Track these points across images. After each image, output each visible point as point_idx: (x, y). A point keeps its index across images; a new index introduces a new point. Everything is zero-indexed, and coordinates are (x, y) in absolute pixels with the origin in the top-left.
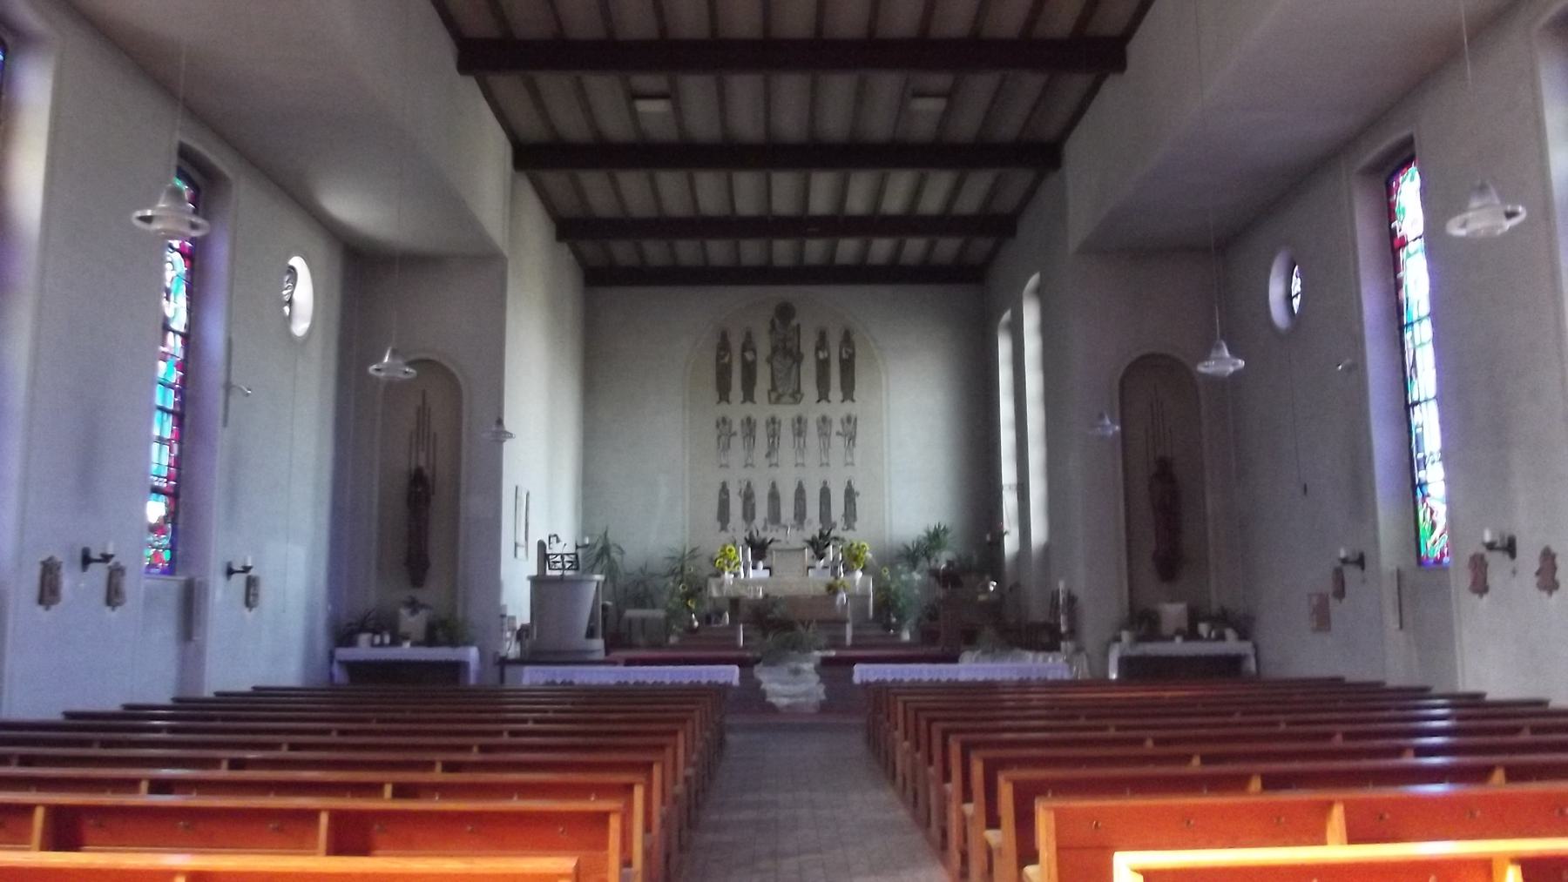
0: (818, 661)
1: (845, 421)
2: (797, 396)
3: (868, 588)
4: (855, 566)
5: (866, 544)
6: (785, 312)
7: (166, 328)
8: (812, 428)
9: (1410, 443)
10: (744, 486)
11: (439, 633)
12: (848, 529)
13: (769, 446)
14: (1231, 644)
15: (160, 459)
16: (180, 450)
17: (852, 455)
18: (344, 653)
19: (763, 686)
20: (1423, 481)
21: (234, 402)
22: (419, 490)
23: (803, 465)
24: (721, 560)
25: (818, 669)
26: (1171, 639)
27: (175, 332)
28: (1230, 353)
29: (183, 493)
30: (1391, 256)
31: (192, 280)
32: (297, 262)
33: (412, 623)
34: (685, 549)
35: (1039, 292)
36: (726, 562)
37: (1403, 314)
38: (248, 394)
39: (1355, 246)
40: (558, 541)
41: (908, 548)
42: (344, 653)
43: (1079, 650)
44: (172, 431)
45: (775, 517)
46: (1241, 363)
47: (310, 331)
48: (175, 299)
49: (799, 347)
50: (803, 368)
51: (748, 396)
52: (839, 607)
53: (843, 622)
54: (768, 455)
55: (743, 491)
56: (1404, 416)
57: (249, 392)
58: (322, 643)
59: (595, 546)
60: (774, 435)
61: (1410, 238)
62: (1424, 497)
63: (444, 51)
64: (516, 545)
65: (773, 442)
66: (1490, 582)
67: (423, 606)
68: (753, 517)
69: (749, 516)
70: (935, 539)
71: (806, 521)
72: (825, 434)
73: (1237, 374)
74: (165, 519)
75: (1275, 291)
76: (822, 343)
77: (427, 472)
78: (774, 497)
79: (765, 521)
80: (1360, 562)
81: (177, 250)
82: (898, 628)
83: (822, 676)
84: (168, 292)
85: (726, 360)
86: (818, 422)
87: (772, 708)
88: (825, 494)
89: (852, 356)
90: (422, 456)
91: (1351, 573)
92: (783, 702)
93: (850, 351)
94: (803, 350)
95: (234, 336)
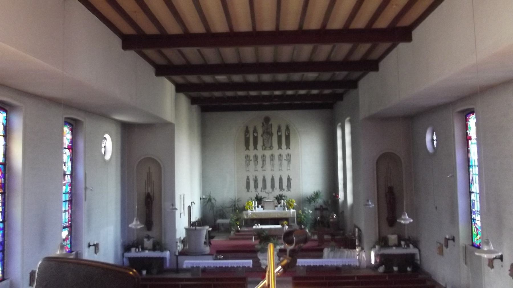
0: (278, 251)
2: (271, 147)
4: (290, 207)
6: (267, 120)
7: (65, 175)
8: (276, 158)
9: (471, 204)
10: (254, 178)
11: (157, 247)
13: (262, 164)
14: (412, 250)
15: (65, 217)
16: (72, 211)
17: (289, 167)
18: (128, 255)
20: (474, 218)
21: (88, 192)
23: (274, 170)
24: (247, 206)
26: (392, 247)
27: (67, 175)
30: (466, 141)
32: (107, 136)
33: (148, 243)
34: (235, 199)
35: (351, 122)
36: (249, 206)
37: (469, 162)
38: (92, 190)
40: (194, 204)
42: (128, 255)
43: (362, 249)
45: (264, 187)
46: (412, 221)
48: (67, 164)
50: (273, 138)
51: (255, 148)
54: (262, 167)
55: (254, 179)
56: (469, 195)
57: (92, 189)
58: (120, 252)
60: (264, 161)
63: (151, 70)
64: (181, 214)
66: (494, 265)
68: (257, 187)
71: (275, 189)
73: (410, 223)
74: (68, 235)
75: (428, 138)
76: (279, 130)
77: (151, 194)
78: (264, 180)
79: (261, 188)
80: (453, 239)
81: (67, 148)
82: (305, 228)
84: (65, 163)
85: (248, 136)
86: (278, 156)
88: (281, 179)
89: (289, 134)
91: (450, 242)
93: (288, 132)
95: (87, 172)
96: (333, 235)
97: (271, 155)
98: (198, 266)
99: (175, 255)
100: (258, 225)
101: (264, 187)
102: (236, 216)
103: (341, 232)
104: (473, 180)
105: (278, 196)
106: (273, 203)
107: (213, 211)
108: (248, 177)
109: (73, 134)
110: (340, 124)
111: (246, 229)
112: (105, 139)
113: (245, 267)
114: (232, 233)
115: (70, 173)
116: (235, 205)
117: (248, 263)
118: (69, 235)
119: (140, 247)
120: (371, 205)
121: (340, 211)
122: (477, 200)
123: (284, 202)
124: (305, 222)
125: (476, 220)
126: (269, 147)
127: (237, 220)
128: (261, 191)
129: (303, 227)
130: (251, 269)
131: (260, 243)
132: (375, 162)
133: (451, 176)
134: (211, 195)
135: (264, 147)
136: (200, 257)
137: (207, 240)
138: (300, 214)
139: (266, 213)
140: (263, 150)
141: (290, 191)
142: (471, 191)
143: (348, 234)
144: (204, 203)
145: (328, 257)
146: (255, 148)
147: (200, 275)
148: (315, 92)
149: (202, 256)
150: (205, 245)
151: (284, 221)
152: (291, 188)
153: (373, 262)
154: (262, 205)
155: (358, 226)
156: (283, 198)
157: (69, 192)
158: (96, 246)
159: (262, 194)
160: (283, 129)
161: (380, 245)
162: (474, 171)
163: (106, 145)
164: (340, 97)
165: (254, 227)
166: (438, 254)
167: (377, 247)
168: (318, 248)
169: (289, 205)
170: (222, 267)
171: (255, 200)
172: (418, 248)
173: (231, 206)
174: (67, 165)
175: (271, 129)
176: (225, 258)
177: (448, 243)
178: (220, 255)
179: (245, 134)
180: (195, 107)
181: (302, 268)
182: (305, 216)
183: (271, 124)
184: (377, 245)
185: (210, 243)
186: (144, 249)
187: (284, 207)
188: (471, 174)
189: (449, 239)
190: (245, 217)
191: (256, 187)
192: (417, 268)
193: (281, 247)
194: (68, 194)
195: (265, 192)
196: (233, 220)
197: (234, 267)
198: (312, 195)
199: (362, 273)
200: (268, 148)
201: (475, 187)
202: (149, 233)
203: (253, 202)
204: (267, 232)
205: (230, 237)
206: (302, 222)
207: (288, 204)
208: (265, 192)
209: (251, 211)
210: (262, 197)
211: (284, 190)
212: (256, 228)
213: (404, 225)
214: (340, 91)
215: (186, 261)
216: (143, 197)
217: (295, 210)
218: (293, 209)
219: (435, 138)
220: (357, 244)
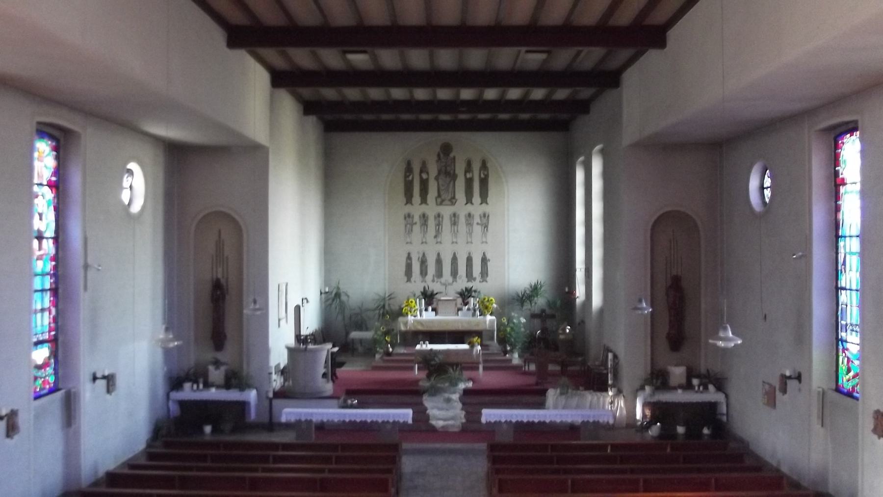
0: (462, 392)
1: (482, 216)
2: (453, 200)
3: (494, 326)
5: (493, 300)
6: (446, 149)
8: (462, 220)
11: (233, 381)
12: (483, 281)
14: (712, 395)
15: (42, 323)
17: (486, 237)
19: (428, 412)
20: (844, 338)
21: (91, 274)
22: (218, 293)
24: (406, 308)
25: (461, 399)
26: (674, 389)
27: (47, 238)
28: (733, 334)
29: (61, 339)
31: (58, 203)
32: (133, 166)
33: (216, 375)
35: (603, 152)
36: (409, 309)
38: (99, 270)
39: (810, 179)
40: (307, 302)
41: (518, 296)
43: (619, 392)
44: (50, 301)
47: (144, 207)
49: (455, 170)
51: (424, 200)
52: (475, 356)
53: (478, 363)
54: (436, 237)
57: (100, 268)
58: (161, 391)
59: (332, 292)
60: (439, 225)
61: (848, 181)
62: (844, 350)
63: (218, 36)
64: (279, 320)
65: (439, 228)
67: (223, 364)
68: (426, 274)
69: (424, 274)
70: (535, 290)
72: (470, 224)
73: (736, 345)
74: (49, 358)
75: (754, 183)
76: (469, 168)
77: (223, 281)
78: (439, 262)
79: (434, 275)
80: (799, 378)
83: (464, 404)
85: (410, 178)
86: (465, 216)
87: (433, 430)
88: (469, 260)
89: (487, 176)
90: (220, 270)
91: (792, 384)
92: (439, 424)
94: (457, 172)
95: (88, 235)
96: (563, 365)
97: (452, 215)
98: (309, 419)
99: (267, 397)
100: (424, 343)
101: (439, 274)
102: (386, 325)
103: (580, 359)
104: (844, 263)
105: (464, 290)
106: (454, 302)
107: (344, 317)
108: (409, 254)
109: (57, 158)
110: (581, 159)
111: (402, 350)
112: (130, 172)
113: (398, 422)
114: (378, 356)
115: (53, 235)
116: (384, 306)
117: (404, 415)
118: (52, 357)
119: (201, 380)
120: (645, 309)
121: (578, 320)
122: (851, 303)
123: (475, 303)
124: (513, 340)
125: (846, 341)
126: (446, 197)
127: (386, 333)
128: (433, 281)
129: (509, 348)
130: (409, 425)
131: (429, 376)
132: (650, 227)
133: (801, 257)
134: (341, 287)
135: (439, 200)
136: (314, 402)
137: (328, 370)
138: (503, 324)
139: (440, 322)
140: (437, 204)
141: (486, 281)
142: (839, 286)
143: (593, 361)
144: (327, 300)
145: (556, 407)
146: (424, 200)
147: (313, 438)
148: (538, 94)
149: (318, 401)
150: (324, 380)
151: (474, 337)
152: (487, 275)
153: (639, 415)
154: (434, 305)
155: (612, 347)
156: (473, 294)
157: (52, 272)
158: (110, 380)
159: (435, 287)
160: (476, 167)
161: (653, 385)
162: (850, 246)
163: (133, 184)
164: (582, 107)
165: (418, 347)
166: (764, 404)
167: (648, 389)
168: (535, 387)
169: (484, 309)
170: (355, 422)
171: (421, 297)
172: (724, 393)
173: (378, 307)
174: (47, 219)
175: (453, 167)
176: (360, 405)
177: (786, 384)
178: (352, 398)
179: (406, 173)
180: (312, 119)
181: (505, 426)
182: (512, 329)
183: (454, 158)
184: (647, 385)
185: (334, 374)
186: (207, 385)
187: (475, 311)
188: (841, 253)
189: (790, 378)
190: (403, 328)
191: (424, 272)
192: (721, 430)
193: (467, 384)
194: (49, 277)
195: (441, 282)
196: (379, 333)
197: (377, 422)
198: (527, 290)
199: (621, 438)
200: (447, 202)
201: (851, 277)
202: (220, 356)
203: (418, 300)
204: (441, 357)
205: (374, 364)
206: (507, 339)
207: (482, 305)
208: (441, 282)
209: (413, 318)
210: (435, 292)
211: (475, 279)
212: (422, 349)
213: (725, 350)
214: (585, 93)
215: (287, 410)
216: (208, 287)
217: (494, 318)
218: (491, 315)
219: (768, 182)
220: (610, 382)
